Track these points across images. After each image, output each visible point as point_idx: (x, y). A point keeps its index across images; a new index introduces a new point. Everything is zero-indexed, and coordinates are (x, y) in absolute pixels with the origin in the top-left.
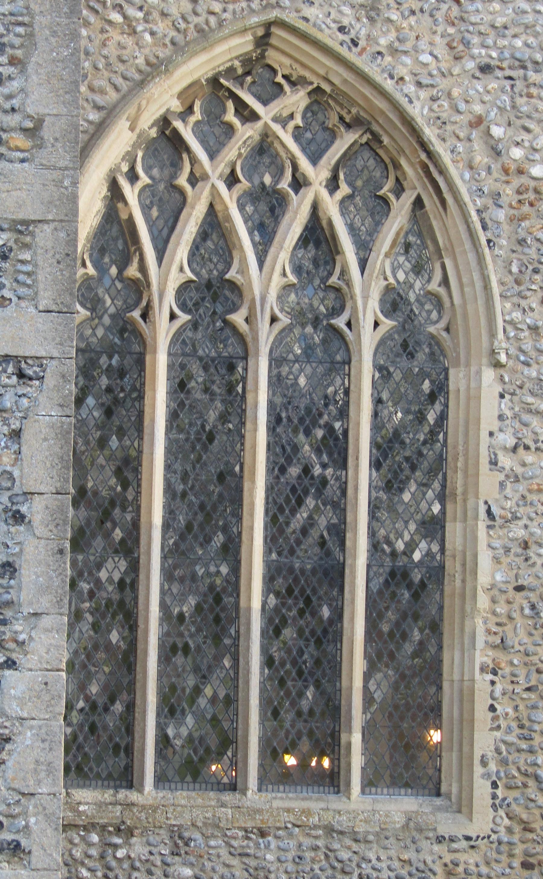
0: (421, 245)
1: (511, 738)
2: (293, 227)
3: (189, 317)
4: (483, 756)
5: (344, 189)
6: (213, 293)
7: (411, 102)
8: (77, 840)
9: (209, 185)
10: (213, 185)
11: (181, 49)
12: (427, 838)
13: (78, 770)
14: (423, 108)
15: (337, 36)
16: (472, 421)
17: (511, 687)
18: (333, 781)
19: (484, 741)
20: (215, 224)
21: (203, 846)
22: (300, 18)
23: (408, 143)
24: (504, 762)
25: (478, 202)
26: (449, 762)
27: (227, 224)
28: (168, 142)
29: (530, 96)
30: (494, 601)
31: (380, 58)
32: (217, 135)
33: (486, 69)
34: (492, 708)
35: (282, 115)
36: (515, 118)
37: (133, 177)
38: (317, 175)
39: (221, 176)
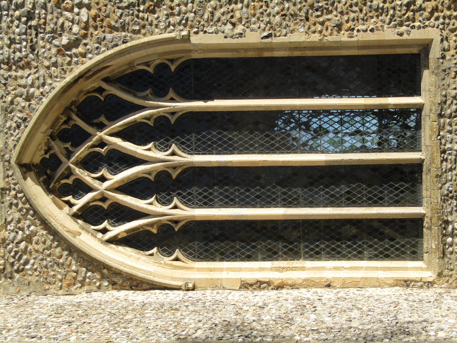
1: (387, 19)
3: (175, 198)
4: (398, 34)
5: (102, 119)
6: (160, 185)
7: (53, 88)
8: (451, 249)
9: (105, 191)
10: (105, 190)
12: (443, 63)
14: (56, 81)
15: (22, 129)
17: (360, 21)
20: (128, 188)
21: (451, 183)
22: (14, 149)
23: (75, 89)
24: (401, 24)
25: (104, 49)
27: (125, 181)
29: (45, 24)
30: (314, 32)
31: (31, 105)
34: (372, 30)
36: (56, 33)
37: (104, 231)
39: (100, 185)
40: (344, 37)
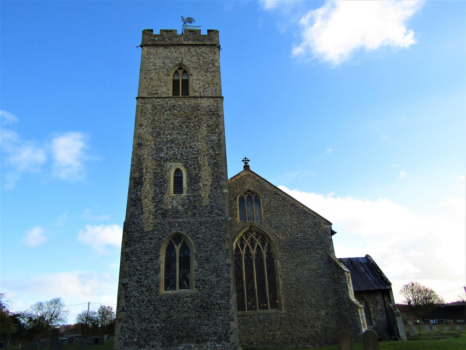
0: (269, 248)
2: (256, 247)
6: (248, 254)
11: (242, 229)
13: (239, 310)
16: (277, 265)
18: (266, 308)
19: (283, 302)
20: (248, 247)
26: (279, 304)
28: (241, 239)
32: (247, 238)
33: (274, 228)
35: (253, 235)
36: (277, 233)
38: (258, 241)
40: (281, 292)
